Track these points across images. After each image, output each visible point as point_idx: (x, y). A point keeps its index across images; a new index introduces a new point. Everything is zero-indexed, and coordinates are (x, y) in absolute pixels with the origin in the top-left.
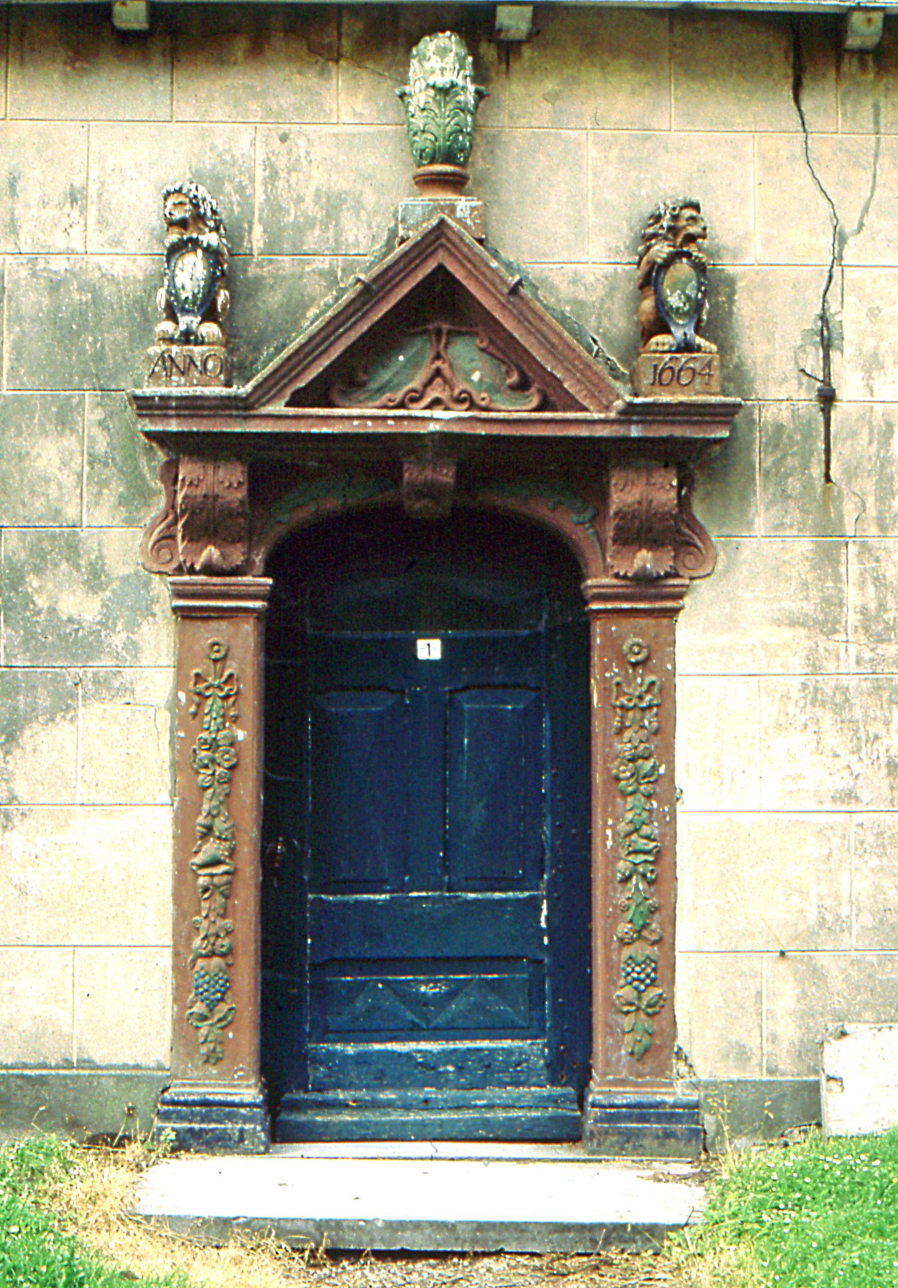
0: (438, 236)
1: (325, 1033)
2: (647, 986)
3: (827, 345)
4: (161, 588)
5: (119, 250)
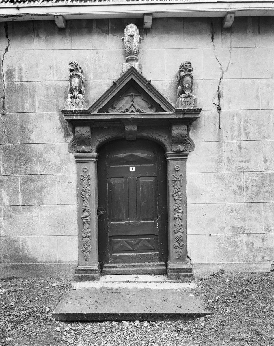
0: (132, 70)
2: (181, 242)
3: (219, 97)
4: (72, 156)
5: (61, 80)
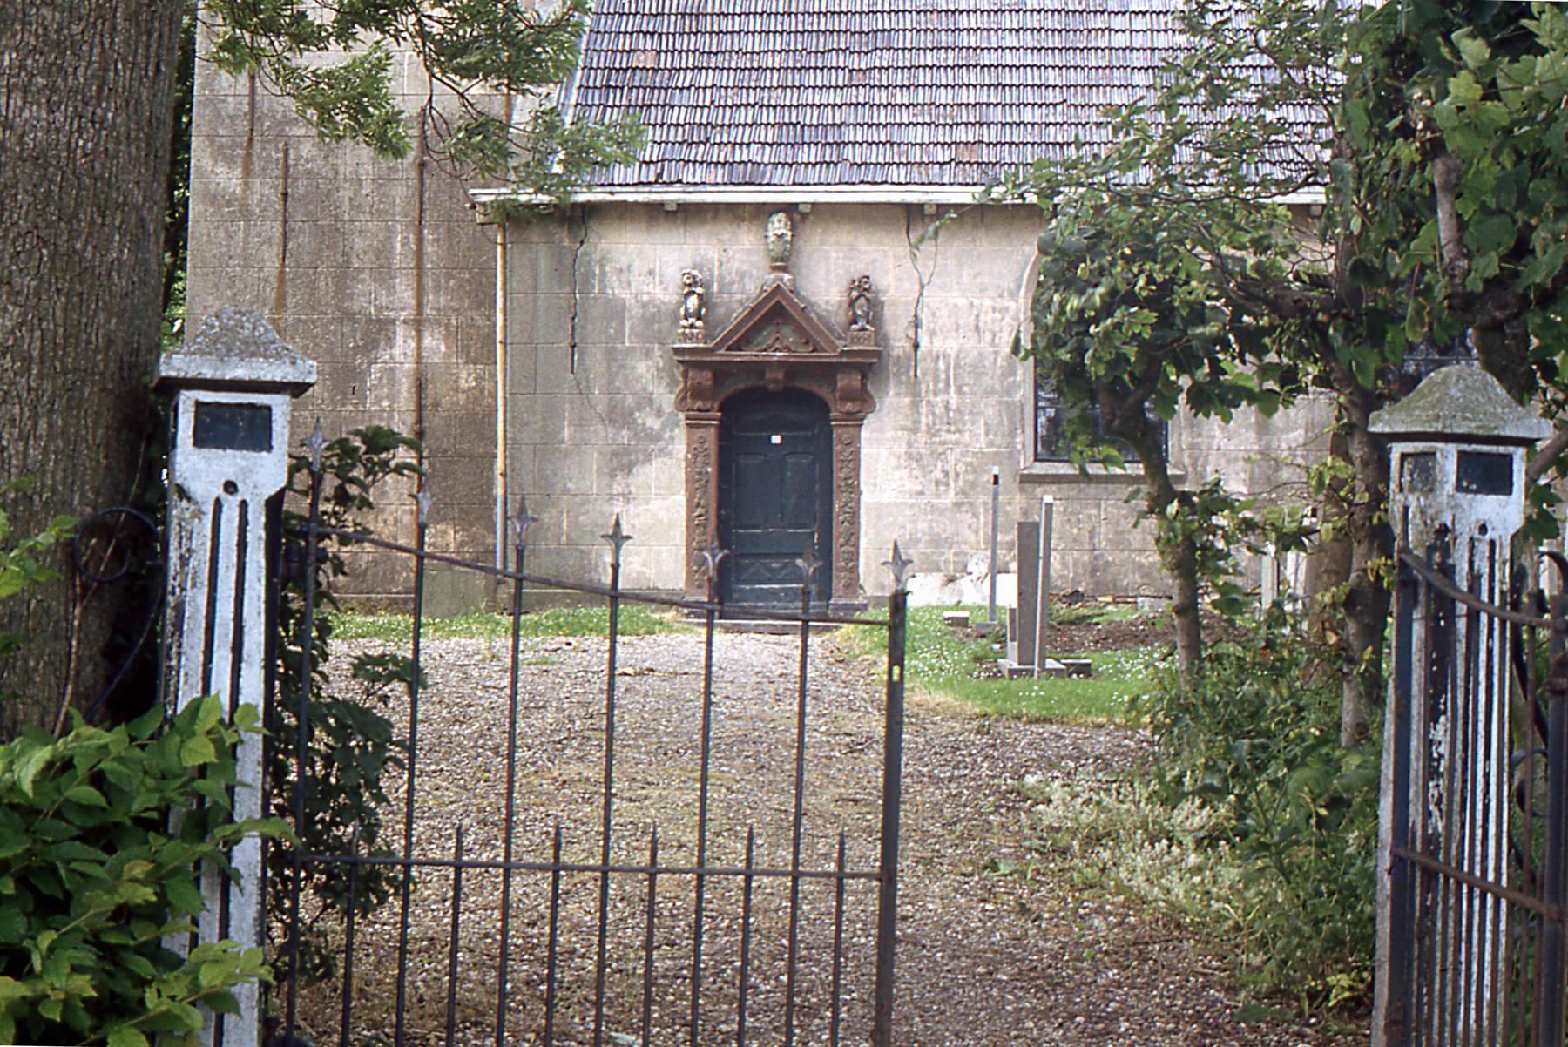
1: (739, 581)
4: (682, 416)
